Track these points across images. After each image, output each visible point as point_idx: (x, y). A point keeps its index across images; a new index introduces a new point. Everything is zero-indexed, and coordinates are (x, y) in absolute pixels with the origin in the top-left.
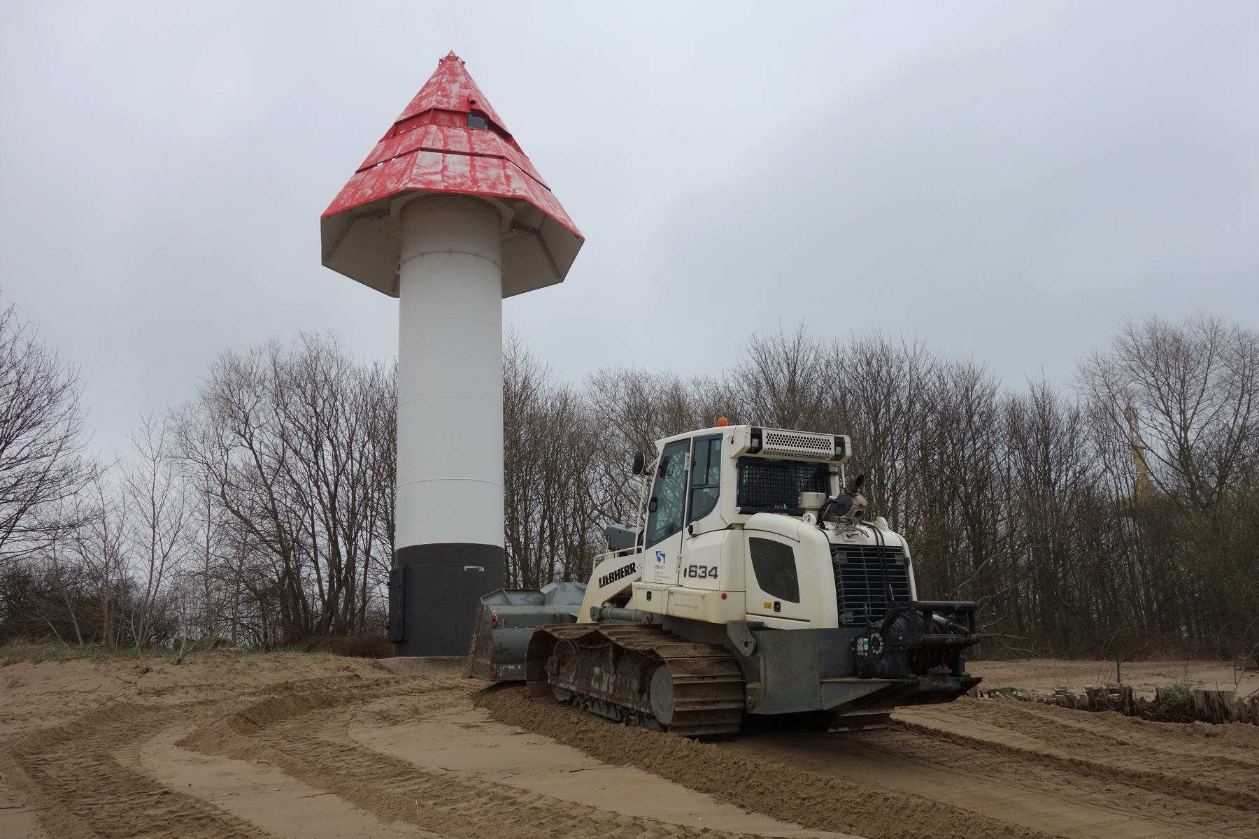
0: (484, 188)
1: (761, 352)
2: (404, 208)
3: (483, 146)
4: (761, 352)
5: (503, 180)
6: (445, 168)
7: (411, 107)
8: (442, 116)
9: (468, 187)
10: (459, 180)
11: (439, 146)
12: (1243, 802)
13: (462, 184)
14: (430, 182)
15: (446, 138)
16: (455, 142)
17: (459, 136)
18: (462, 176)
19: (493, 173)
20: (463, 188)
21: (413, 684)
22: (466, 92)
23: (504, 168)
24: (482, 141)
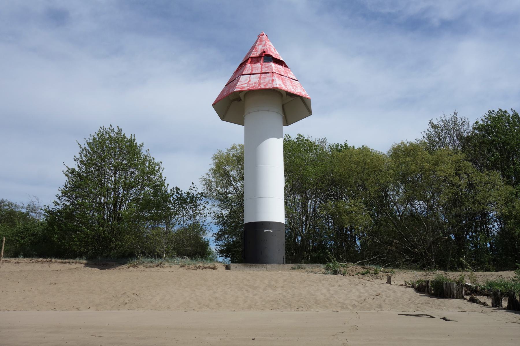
0: (263, 87)
1: (490, 111)
2: (245, 96)
3: (266, 69)
4: (490, 111)
5: (271, 82)
6: (250, 81)
7: (245, 58)
8: (254, 59)
9: (257, 87)
10: (254, 85)
11: (249, 72)
12: (516, 307)
13: (255, 86)
14: (243, 87)
15: (252, 68)
16: (255, 70)
17: (258, 67)
18: (255, 83)
19: (267, 79)
20: (255, 88)
21: (483, 277)
22: (264, 48)
23: (272, 77)
24: (266, 67)
